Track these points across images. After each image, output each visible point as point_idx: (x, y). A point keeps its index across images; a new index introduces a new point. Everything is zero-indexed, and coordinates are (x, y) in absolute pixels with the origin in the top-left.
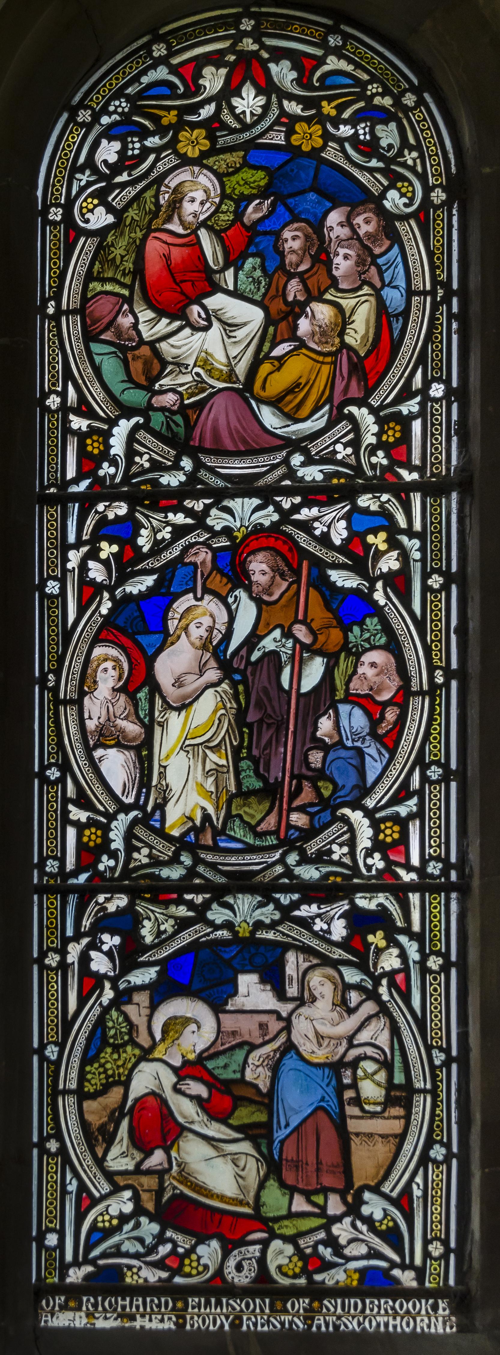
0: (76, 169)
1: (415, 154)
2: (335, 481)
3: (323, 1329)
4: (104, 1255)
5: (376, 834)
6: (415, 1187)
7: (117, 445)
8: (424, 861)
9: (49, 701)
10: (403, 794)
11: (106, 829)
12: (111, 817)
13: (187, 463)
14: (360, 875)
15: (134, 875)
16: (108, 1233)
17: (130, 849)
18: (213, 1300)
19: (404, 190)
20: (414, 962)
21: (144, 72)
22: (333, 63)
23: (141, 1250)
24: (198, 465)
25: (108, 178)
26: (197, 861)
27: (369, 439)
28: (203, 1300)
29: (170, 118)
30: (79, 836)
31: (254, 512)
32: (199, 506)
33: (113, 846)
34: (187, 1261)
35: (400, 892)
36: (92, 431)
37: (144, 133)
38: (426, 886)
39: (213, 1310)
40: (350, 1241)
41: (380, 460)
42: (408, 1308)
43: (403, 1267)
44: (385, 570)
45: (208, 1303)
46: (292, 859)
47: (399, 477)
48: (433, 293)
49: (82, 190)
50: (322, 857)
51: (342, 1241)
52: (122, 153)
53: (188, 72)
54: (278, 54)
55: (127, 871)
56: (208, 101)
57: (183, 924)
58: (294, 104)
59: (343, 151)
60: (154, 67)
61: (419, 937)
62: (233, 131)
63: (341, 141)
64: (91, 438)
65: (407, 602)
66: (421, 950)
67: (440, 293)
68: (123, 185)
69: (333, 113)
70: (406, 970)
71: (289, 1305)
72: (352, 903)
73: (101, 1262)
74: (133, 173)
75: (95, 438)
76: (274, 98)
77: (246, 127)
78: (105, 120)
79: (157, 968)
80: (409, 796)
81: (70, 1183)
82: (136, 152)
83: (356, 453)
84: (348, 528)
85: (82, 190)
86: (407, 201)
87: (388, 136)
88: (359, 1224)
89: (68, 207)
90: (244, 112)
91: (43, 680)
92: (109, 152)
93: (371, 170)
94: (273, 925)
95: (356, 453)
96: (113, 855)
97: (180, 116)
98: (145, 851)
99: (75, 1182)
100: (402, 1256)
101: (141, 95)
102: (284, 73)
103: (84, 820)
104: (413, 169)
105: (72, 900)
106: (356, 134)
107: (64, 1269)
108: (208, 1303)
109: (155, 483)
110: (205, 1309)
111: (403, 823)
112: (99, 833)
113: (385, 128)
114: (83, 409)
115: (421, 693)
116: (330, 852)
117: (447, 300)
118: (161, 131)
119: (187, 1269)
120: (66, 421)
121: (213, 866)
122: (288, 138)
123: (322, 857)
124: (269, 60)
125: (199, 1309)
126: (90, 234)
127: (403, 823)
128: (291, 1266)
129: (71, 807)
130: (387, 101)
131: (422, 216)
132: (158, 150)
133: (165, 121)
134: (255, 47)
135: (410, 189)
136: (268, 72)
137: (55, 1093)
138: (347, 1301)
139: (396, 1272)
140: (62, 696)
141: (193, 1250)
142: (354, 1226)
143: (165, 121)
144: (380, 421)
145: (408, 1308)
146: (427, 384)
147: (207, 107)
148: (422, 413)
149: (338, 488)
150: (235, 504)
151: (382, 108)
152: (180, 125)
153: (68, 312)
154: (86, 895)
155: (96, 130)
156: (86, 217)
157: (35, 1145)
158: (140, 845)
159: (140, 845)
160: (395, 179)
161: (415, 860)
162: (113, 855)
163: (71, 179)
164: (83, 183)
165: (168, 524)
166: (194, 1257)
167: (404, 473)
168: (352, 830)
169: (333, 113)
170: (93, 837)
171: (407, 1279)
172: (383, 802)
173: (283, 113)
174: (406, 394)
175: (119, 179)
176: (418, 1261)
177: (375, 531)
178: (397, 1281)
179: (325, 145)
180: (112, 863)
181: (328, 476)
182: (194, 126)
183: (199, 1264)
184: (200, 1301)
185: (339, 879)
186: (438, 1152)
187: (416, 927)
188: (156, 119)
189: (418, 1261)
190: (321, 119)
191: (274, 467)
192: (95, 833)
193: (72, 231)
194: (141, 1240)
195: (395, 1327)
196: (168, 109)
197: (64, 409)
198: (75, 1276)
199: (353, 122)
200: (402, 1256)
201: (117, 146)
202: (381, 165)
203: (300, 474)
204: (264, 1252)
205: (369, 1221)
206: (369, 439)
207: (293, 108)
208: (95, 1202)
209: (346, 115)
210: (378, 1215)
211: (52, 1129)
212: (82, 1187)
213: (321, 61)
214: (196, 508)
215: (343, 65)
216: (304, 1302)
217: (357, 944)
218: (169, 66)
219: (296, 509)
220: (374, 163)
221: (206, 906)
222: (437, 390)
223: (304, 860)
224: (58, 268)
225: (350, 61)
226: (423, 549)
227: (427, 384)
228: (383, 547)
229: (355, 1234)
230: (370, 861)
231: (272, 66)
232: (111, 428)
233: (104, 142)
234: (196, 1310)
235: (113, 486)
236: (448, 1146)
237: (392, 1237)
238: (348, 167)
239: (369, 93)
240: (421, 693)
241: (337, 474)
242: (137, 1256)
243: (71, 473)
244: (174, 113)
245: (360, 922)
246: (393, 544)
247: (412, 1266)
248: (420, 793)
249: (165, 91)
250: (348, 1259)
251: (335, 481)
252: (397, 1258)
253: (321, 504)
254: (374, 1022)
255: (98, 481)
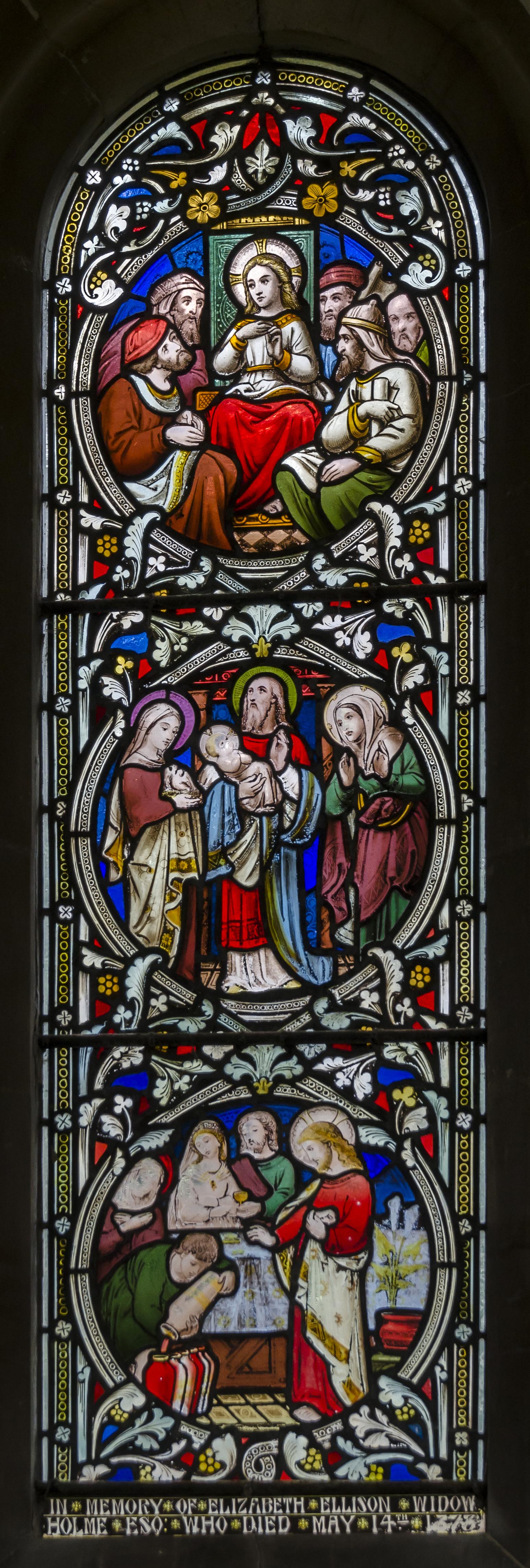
0: (85, 235)
1: (439, 224)
2: (357, 585)
3: (337, 1530)
4: (122, 1450)
5: (407, 977)
6: (438, 1369)
7: (133, 547)
8: (454, 1007)
9: (59, 833)
10: (431, 934)
11: (122, 975)
12: (128, 962)
14: (390, 1025)
15: (151, 1026)
16: (122, 1427)
17: (148, 995)
18: (343, 1499)
19: (426, 264)
20: (443, 1120)
21: (154, 130)
22: (355, 119)
23: (156, 1446)
25: (117, 247)
26: (219, 1010)
28: (334, 1500)
29: (179, 180)
30: (94, 985)
31: (275, 621)
32: (217, 614)
34: (202, 1458)
35: (428, 1042)
36: (105, 530)
37: (155, 198)
38: (456, 1034)
39: (344, 1510)
40: (369, 1433)
41: (121, 575)
42: (449, 1506)
43: (429, 1462)
44: (411, 686)
45: (339, 1503)
47: (426, 580)
49: (90, 259)
51: (360, 1433)
52: (131, 220)
53: (198, 129)
54: (297, 111)
55: (144, 1022)
56: (219, 162)
57: (200, 1082)
59: (360, 217)
60: (164, 124)
61: (447, 1093)
62: (244, 195)
63: (359, 206)
64: (102, 538)
65: (433, 720)
66: (450, 1107)
68: (132, 255)
70: (432, 1130)
71: (178, 1506)
72: (379, 1055)
73: (114, 1460)
74: (140, 243)
75: (107, 538)
78: (118, 181)
79: (170, 1132)
80: (438, 936)
81: (82, 1372)
82: (145, 216)
83: (381, 554)
84: (373, 640)
85: (90, 259)
88: (378, 1413)
91: (51, 809)
92: (117, 219)
93: (390, 240)
94: (293, 1082)
95: (381, 554)
97: (189, 179)
98: (163, 998)
99: (88, 1371)
100: (425, 1448)
101: (150, 155)
102: (299, 131)
105: (86, 1055)
106: (376, 199)
107: (77, 1469)
108: (339, 1503)
109: (172, 587)
110: (225, 1510)
115: (448, 822)
116: (359, 1000)
117: (474, 386)
118: (171, 194)
119: (203, 1467)
120: (77, 518)
121: (234, 1016)
122: (299, 203)
124: (286, 116)
125: (331, 1509)
128: (310, 1460)
129: (85, 951)
130: (410, 165)
132: (167, 216)
133: (174, 185)
134: (271, 101)
135: (433, 262)
136: (283, 128)
137: (67, 1272)
138: (432, 1498)
139: (422, 1466)
140: (73, 828)
141: (208, 1444)
142: (372, 1416)
143: (174, 185)
145: (449, 1506)
146: (452, 479)
147: (217, 168)
148: (449, 511)
149: (363, 593)
150: (253, 611)
151: (402, 172)
152: (189, 190)
154: (101, 1049)
155: (109, 193)
158: (158, 992)
159: (158, 992)
160: (417, 252)
161: (445, 1009)
163: (79, 247)
164: (90, 253)
165: (184, 634)
166: (209, 1452)
167: (430, 576)
168: (381, 973)
169: (352, 174)
171: (433, 1473)
173: (296, 174)
174: (430, 491)
175: (126, 249)
176: (443, 1453)
177: (398, 643)
178: (423, 1475)
179: (340, 211)
182: (204, 189)
183: (215, 1461)
184: (331, 1500)
186: (463, 1333)
187: (445, 1082)
189: (443, 1453)
191: (292, 571)
194: (154, 1436)
195: (208, 1528)
197: (75, 505)
198: (91, 1474)
199: (371, 184)
200: (425, 1448)
201: (126, 210)
202: (402, 232)
204: (280, 1447)
205: (389, 1410)
207: (309, 169)
208: (110, 1392)
209: (364, 177)
210: (398, 1401)
211: (64, 1311)
212: (95, 1376)
213: (342, 118)
214: (304, 612)
215: (365, 121)
216: (192, 1502)
217: (382, 1102)
218: (180, 122)
219: (318, 618)
220: (395, 231)
221: (227, 1058)
222: (463, 486)
224: (66, 347)
225: (373, 119)
226: (450, 663)
227: (452, 479)
228: (408, 658)
229: (373, 1425)
231: (289, 123)
232: (125, 527)
234: (281, 1511)
235: (128, 592)
236: (475, 1326)
237: (412, 1425)
239: (390, 155)
240: (448, 822)
241: (360, 579)
242: (151, 1453)
243: (82, 578)
244: (183, 175)
245: (388, 1077)
246: (420, 657)
247: (437, 1461)
248: (450, 932)
249: (176, 150)
250: (369, 1451)
251: (357, 585)
252: (421, 1453)
253: (345, 613)
255: (112, 587)
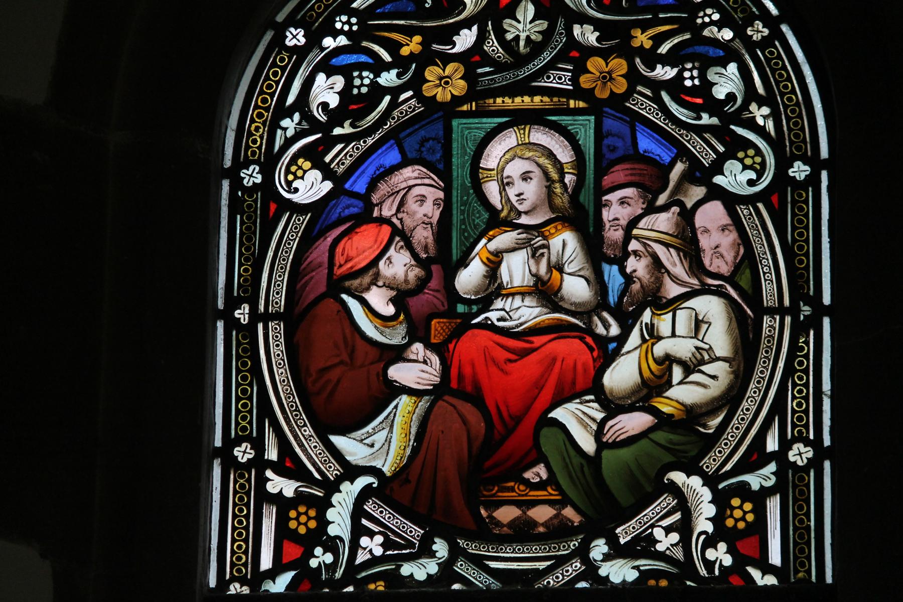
2: (652, 582)
7: (339, 522)
12: (332, 487)
13: (441, 548)
19: (748, 161)
24: (455, 552)
27: (703, 525)
29: (412, 46)
33: (332, 530)
46: (599, 549)
48: (794, 310)
50: (642, 546)
52: (344, 94)
56: (467, 24)
58: (589, 28)
63: (657, 85)
67: (806, 310)
68: (346, 139)
69: (648, 44)
76: (561, 23)
77: (520, 61)
82: (364, 90)
83: (685, 542)
85: (289, 142)
86: (753, 176)
87: (726, 82)
89: (268, 171)
90: (517, 38)
92: (327, 91)
93: (700, 130)
96: (331, 545)
103: (289, 493)
104: (761, 131)
111: (759, 498)
112: (312, 513)
113: (723, 71)
114: (289, 466)
120: (262, 481)
123: (642, 546)
126: (300, 209)
127: (759, 498)
131: (775, 199)
132: (395, 92)
133: (405, 51)
135: (758, 159)
144: (721, 500)
148: (780, 488)
152: (426, 58)
153: (267, 318)
156: (295, 185)
157: (217, 453)
160: (735, 147)
162: (331, 545)
163: (274, 125)
164: (290, 133)
169: (648, 44)
170: (303, 519)
172: (728, 467)
173: (572, 42)
174: (755, 458)
180: (329, 558)
181: (645, 575)
182: (447, 59)
185: (664, 583)
188: (393, 47)
190: (628, 52)
192: (306, 513)
193: (272, 204)
196: (409, 32)
197: (260, 463)
201: (339, 82)
203: (603, 572)
206: (703, 525)
207: (588, 35)
209: (664, 49)
223: (617, 552)
227: (785, 444)
230: (711, 554)
233: (321, 77)
238: (670, 128)
239: (699, 21)
241: (656, 574)
251: (652, 582)
254: (720, 363)
